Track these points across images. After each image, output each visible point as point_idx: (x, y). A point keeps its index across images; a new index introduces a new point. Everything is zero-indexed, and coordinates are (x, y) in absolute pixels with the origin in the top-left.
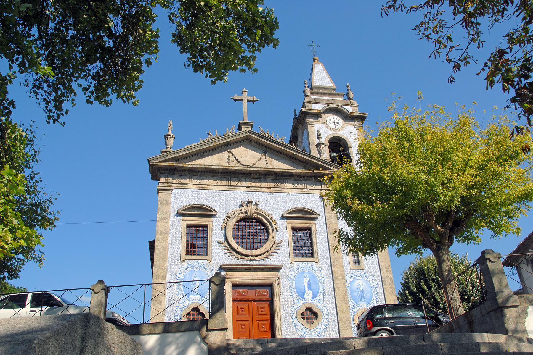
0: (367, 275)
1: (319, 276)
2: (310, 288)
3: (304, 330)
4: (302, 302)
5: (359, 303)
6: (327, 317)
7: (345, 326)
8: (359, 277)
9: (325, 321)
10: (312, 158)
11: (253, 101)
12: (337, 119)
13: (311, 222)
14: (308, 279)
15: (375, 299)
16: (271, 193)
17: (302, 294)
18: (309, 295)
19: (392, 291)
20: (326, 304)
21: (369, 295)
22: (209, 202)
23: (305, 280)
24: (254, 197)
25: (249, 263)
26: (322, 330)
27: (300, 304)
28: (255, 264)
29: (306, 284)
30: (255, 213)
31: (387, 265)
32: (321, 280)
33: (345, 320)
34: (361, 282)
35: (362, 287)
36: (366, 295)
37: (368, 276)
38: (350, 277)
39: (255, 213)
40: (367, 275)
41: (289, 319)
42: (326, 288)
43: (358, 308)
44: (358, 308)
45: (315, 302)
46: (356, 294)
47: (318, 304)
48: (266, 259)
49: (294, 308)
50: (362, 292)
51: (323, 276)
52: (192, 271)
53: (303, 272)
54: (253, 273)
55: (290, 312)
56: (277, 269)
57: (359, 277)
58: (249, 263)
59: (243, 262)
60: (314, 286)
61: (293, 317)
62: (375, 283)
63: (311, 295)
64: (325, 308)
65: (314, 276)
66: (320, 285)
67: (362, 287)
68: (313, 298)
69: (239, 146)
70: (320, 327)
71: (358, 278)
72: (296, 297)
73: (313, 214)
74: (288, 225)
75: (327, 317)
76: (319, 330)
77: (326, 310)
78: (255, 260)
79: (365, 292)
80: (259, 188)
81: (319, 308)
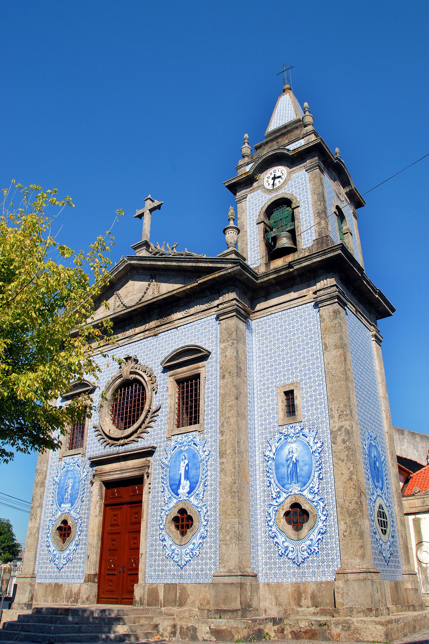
0: (306, 431)
1: (201, 453)
2: (187, 477)
3: (173, 547)
4: (175, 501)
5: (288, 486)
6: (205, 523)
7: (228, 538)
8: (292, 437)
9: (202, 530)
10: (198, 262)
11: (159, 207)
12: (280, 170)
13: (200, 364)
14: (187, 462)
15: (316, 474)
16: (155, 335)
17: (175, 488)
18: (183, 490)
19: (347, 456)
20: (207, 500)
21: (306, 468)
22: (205, 344)
23: (182, 463)
24: (131, 350)
25: (122, 449)
26: (196, 545)
27: (171, 505)
28: (121, 451)
29: (182, 472)
30: (131, 373)
31: (342, 405)
32: (203, 460)
33: (228, 528)
34: (294, 446)
35: (295, 455)
36: (301, 470)
37: (307, 434)
38: (277, 439)
39: (131, 373)
40: (306, 431)
41: (156, 531)
42: (209, 473)
43: (285, 495)
44: (285, 495)
45: (192, 499)
46: (284, 470)
47: (195, 502)
48: (139, 439)
49: (164, 512)
50: (295, 465)
51: (206, 453)
52: (67, 471)
53: (181, 452)
54: (123, 463)
55: (159, 518)
56: (149, 452)
57: (292, 437)
58: (122, 449)
59: (115, 449)
60: (192, 473)
61: (162, 527)
62: (319, 445)
63: (187, 489)
64: (204, 508)
65: (194, 456)
66: (201, 468)
67: (295, 455)
68: (189, 493)
69: (127, 282)
70: (195, 541)
71: (289, 440)
72: (168, 493)
73: (199, 351)
74: (171, 379)
75: (205, 523)
76: (191, 546)
77: (205, 510)
78: (126, 444)
79: (300, 464)
80: (142, 334)
81: (196, 509)
